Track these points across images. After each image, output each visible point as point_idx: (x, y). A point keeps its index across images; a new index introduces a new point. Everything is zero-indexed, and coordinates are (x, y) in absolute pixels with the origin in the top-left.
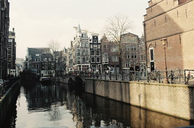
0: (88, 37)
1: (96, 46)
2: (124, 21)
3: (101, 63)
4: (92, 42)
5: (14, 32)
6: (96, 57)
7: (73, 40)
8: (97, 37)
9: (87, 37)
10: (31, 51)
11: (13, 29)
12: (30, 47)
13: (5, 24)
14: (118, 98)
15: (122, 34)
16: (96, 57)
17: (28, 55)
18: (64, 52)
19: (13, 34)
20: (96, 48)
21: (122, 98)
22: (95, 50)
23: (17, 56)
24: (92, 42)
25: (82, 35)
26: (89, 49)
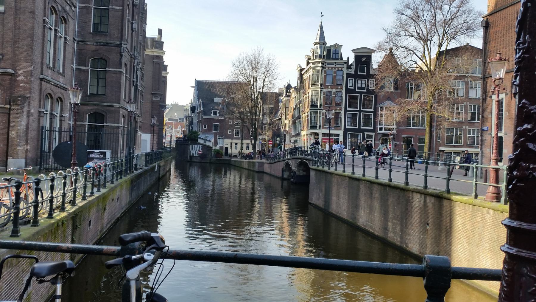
0: (345, 58)
1: (363, 82)
2: (454, 10)
3: (374, 130)
4: (352, 71)
5: (162, 40)
6: (360, 111)
7: (304, 65)
8: (369, 58)
9: (341, 58)
10: (203, 89)
11: (160, 31)
12: (199, 79)
13: (133, 20)
14: (376, 228)
15: (443, 49)
16: (360, 111)
17: (197, 98)
18: (284, 94)
19: (159, 44)
20: (364, 88)
21: (385, 229)
22: (361, 93)
23: (170, 101)
24: (352, 71)
25: (329, 51)
26: (344, 91)
